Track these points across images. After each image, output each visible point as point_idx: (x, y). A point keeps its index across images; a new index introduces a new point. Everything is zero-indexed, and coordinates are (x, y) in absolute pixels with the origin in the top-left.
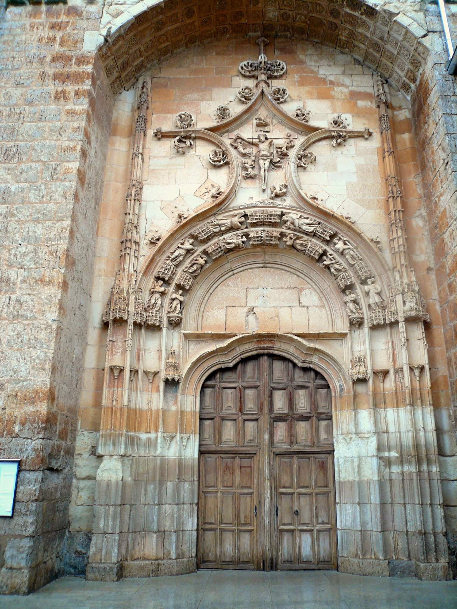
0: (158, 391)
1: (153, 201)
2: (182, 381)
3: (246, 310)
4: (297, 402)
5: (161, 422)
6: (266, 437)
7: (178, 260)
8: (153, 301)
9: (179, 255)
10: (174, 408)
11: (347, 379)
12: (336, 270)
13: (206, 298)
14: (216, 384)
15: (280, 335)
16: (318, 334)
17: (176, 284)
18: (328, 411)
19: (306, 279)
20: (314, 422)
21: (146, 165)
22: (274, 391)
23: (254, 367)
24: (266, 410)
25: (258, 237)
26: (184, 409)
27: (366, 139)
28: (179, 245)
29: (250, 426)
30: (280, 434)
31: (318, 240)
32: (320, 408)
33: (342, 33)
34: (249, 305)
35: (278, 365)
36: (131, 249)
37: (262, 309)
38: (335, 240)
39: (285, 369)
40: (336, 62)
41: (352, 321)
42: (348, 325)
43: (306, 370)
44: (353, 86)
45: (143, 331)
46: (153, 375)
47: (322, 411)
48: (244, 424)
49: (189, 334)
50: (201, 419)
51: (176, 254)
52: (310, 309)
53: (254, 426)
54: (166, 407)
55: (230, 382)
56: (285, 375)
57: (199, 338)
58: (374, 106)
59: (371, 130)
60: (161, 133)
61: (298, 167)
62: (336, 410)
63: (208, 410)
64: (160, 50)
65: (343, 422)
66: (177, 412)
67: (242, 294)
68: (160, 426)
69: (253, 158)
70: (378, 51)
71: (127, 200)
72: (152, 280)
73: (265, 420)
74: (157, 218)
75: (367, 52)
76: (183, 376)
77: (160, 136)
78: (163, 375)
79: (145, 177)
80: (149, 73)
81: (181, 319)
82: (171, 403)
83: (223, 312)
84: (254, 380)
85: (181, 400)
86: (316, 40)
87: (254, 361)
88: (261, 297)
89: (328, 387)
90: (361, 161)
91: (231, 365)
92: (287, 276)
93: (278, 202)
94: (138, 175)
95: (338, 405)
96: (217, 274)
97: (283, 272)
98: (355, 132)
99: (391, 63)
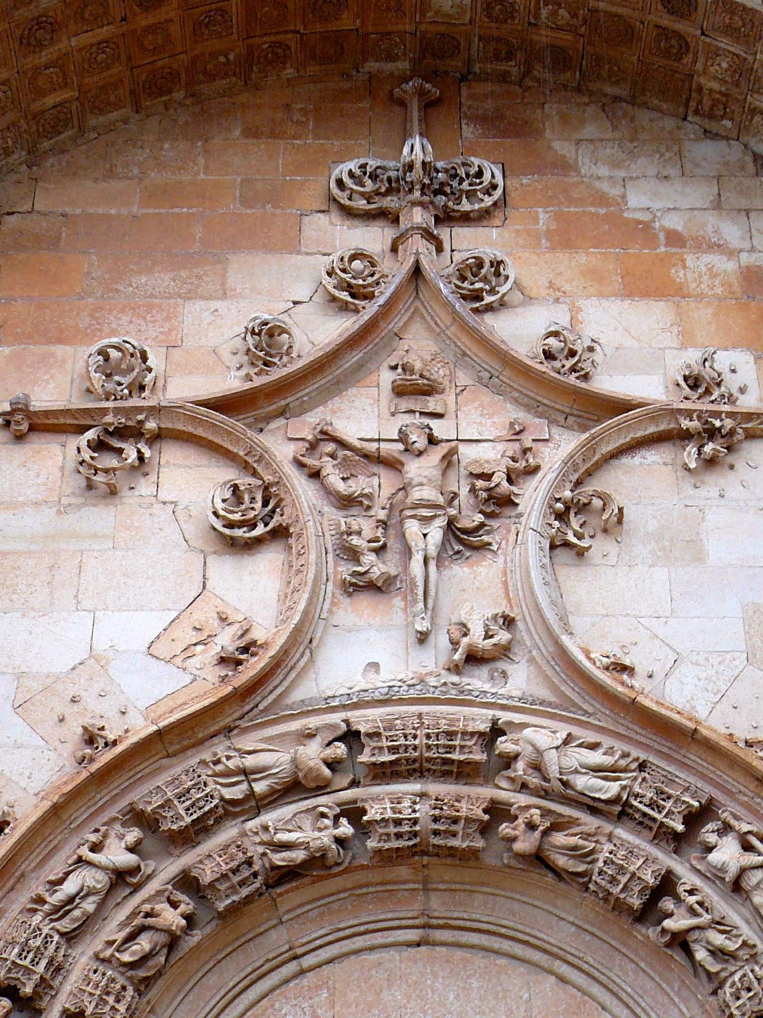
7: (77, 913)
9: (84, 893)
12: (717, 953)
25: (398, 822)
38: (708, 833)
40: (688, 166)
44: (753, 249)
60: (29, 414)
93: (478, 681)
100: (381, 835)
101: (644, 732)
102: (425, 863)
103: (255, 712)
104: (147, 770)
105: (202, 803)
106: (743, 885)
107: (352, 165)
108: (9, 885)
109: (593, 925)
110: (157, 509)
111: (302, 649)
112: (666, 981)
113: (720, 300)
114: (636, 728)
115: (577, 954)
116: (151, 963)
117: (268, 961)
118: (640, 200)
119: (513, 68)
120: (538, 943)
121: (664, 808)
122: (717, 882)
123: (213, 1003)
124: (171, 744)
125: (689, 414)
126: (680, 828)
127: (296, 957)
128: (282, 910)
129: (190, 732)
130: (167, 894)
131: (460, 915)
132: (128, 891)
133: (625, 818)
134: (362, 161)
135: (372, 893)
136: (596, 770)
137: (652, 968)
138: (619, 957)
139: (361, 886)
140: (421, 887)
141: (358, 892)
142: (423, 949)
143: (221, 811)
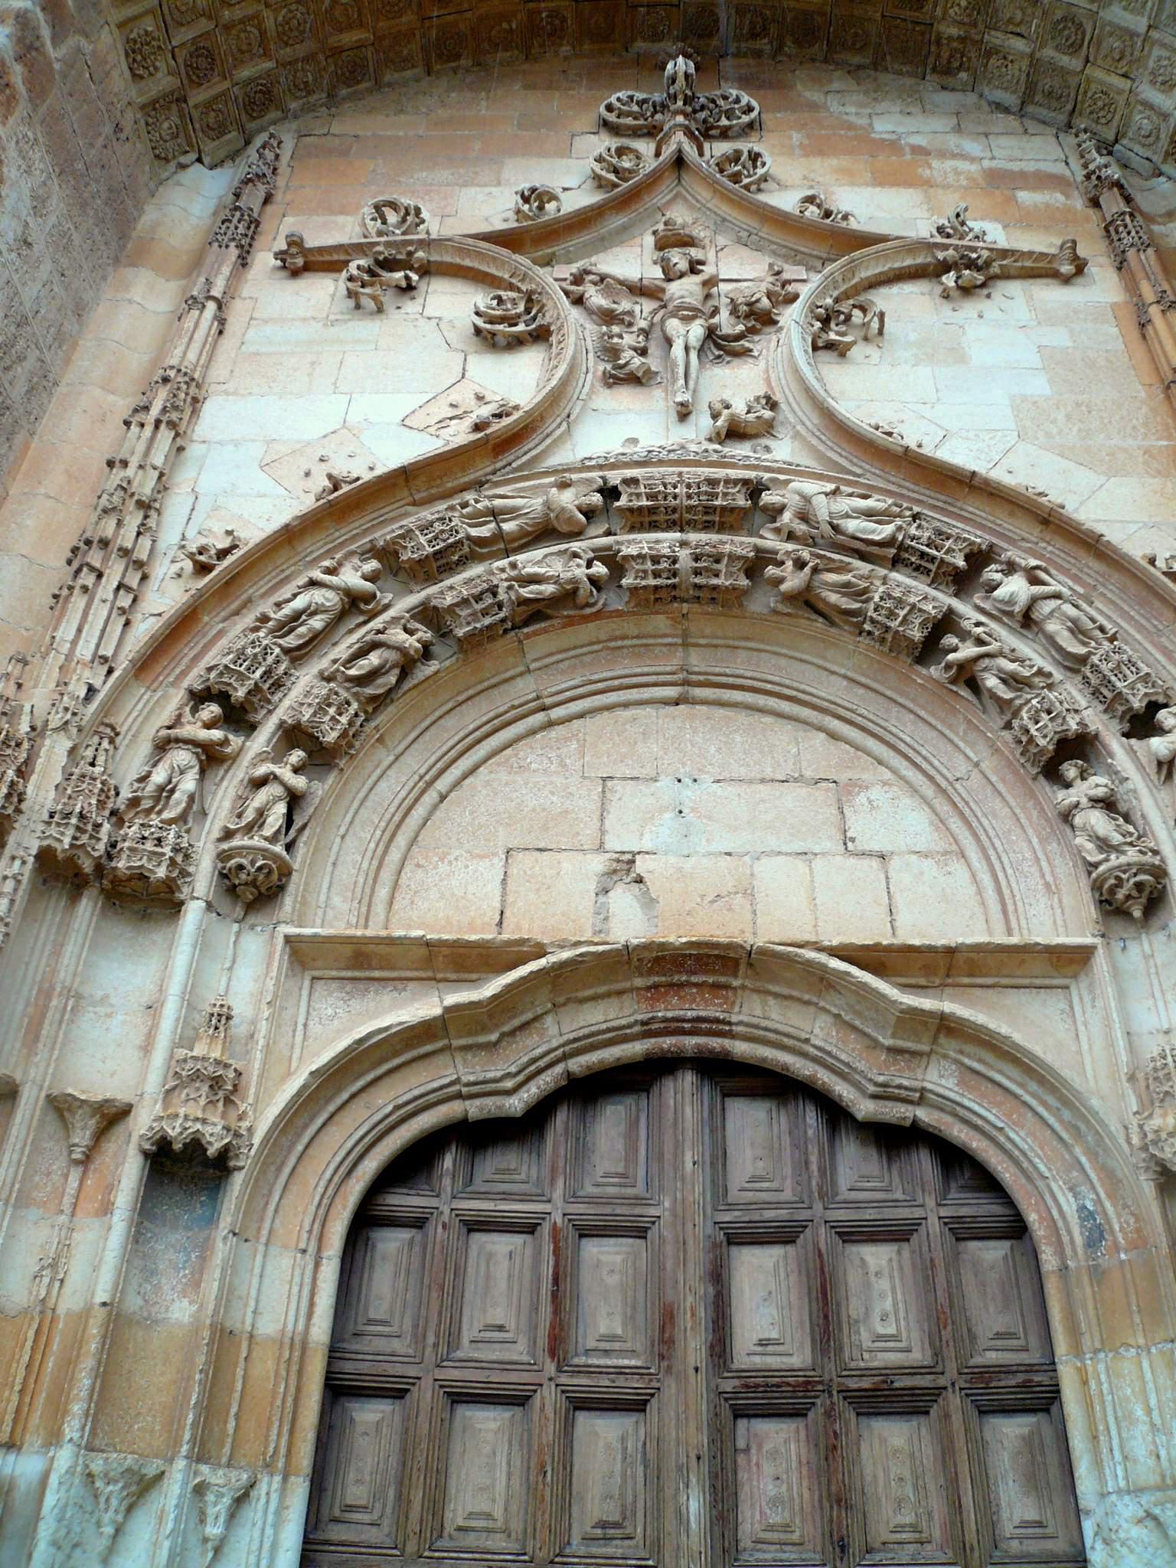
0: (106, 1209)
1: (236, 443)
2: (246, 1161)
3: (598, 864)
4: (854, 1308)
5: (84, 1381)
6: (695, 1505)
7: (302, 630)
8: (159, 777)
9: (311, 611)
10: (181, 1311)
11: (1123, 1171)
12: (1011, 680)
13: (420, 811)
14: (433, 1202)
15: (762, 952)
16: (950, 951)
17: (282, 723)
18: (1034, 1357)
19: (871, 743)
20: (957, 1419)
21: (228, 343)
22: (735, 1250)
23: (633, 1125)
24: (694, 1347)
25: (656, 560)
26: (241, 1319)
27: (1067, 280)
28: (317, 574)
29: (603, 1436)
30: (771, 1489)
31: (915, 578)
32: (983, 1342)
33: (945, 12)
34: (613, 843)
35: (751, 1123)
36: (100, 576)
37: (672, 860)
38: (991, 573)
39: (786, 1140)
40: (928, 107)
41: (1112, 891)
42: (1092, 911)
43: (893, 1140)
44: (993, 158)
45: (87, 907)
46: (92, 1123)
47: (992, 1357)
48: (568, 1426)
49: (315, 939)
50: (339, 1390)
51: (299, 603)
52: (895, 864)
53: (623, 1439)
54: (133, 1303)
55: (506, 1196)
56: (788, 1170)
57: (364, 961)
58: (1079, 203)
59: (1081, 252)
60: (305, 252)
61: (815, 348)
62: (1077, 1350)
63: (380, 1344)
64: (336, 52)
65: (1133, 1421)
66: (195, 1328)
67: (586, 800)
68: (77, 1408)
69: (643, 324)
70: (1074, 48)
71: (127, 423)
72: (177, 697)
73: (685, 1407)
74: (244, 477)
75: (1034, 62)
76: (257, 1141)
77: (302, 262)
78: (142, 1124)
79: (219, 371)
80: (294, 125)
81: (286, 872)
82: (169, 1283)
83: (490, 871)
84: (630, 1191)
85: (231, 1268)
86: (856, 60)
87: (630, 1100)
88: (668, 816)
89: (1016, 1229)
90: (1059, 338)
91: (515, 1105)
92: (782, 735)
93: (740, 450)
94: (192, 356)
95: (1086, 1318)
96: (474, 716)
97: (769, 719)
98: (1023, 253)
99: (1125, 76)
100: (638, 571)
101: (917, 488)
102: (685, 611)
103: (508, 469)
104: (391, 515)
105: (445, 536)
106: (1035, 616)
107: (622, 95)
108: (234, 606)
109: (867, 676)
110: (422, 322)
111: (559, 420)
112: (950, 727)
113: (966, 189)
114: (907, 484)
115: (850, 706)
116: (380, 681)
117: (514, 707)
118: (884, 126)
119: (763, 44)
120: (807, 698)
121: (943, 547)
122: (1005, 619)
123: (451, 743)
124: (418, 491)
125: (946, 247)
126: (961, 563)
127: (544, 709)
128: (529, 657)
129: (439, 481)
130: (403, 621)
131: (722, 670)
132: (361, 619)
133: (900, 566)
134: (630, 93)
135: (627, 647)
136: (869, 514)
137: (933, 715)
138: (895, 709)
139: (615, 639)
140: (680, 641)
141: (613, 644)
142: (681, 707)
143: (466, 549)
